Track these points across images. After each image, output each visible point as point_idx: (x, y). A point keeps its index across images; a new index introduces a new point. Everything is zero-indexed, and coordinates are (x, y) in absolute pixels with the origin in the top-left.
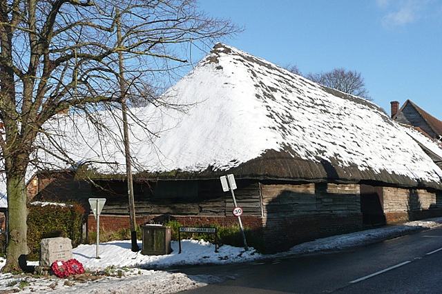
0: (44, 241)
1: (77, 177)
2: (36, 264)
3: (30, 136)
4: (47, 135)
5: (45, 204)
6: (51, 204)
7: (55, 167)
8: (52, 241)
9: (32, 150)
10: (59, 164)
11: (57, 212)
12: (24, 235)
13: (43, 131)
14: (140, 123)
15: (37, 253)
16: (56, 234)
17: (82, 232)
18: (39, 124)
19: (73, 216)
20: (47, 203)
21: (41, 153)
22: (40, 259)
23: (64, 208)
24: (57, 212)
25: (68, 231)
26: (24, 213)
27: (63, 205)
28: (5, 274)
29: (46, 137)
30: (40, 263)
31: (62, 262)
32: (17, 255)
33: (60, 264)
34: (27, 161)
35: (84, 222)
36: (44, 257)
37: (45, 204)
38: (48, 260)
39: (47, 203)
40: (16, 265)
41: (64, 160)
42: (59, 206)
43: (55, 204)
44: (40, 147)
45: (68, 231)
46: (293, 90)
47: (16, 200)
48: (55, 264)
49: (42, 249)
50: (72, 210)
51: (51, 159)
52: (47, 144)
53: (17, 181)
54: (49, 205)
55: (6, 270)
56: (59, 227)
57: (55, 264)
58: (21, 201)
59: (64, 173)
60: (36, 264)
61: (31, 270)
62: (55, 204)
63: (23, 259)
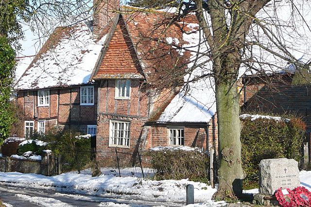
0: (264, 162)
1: (295, 81)
2: (255, 191)
3: (242, 29)
4: (263, 27)
5: (255, 117)
6: (263, 117)
7: (275, 69)
8: (273, 162)
9: (245, 45)
10: (274, 64)
11: (270, 128)
12: (237, 156)
13: (257, 22)
14: (117, 54)
15: (255, 179)
16: (272, 155)
17: (303, 155)
18: (253, 12)
19: (291, 133)
20: (258, 116)
21: (256, 50)
22: (260, 186)
23: (280, 123)
24: (270, 128)
25: (285, 153)
26: (237, 128)
27: (277, 118)
28: (218, 202)
29: (261, 31)
30: (260, 191)
31: (288, 189)
32: (231, 180)
33: (285, 192)
34: (239, 61)
35: (305, 141)
36: (265, 182)
37: (255, 117)
38: (270, 187)
39: (258, 116)
40: (230, 192)
41: (286, 59)
42: (274, 120)
43: (268, 117)
44: (254, 43)
45: (285, 153)
46: (36, 30)
47: (226, 111)
48: (279, 191)
49: (262, 172)
50: (289, 124)
51: (270, 58)
52: (265, 41)
53: (228, 87)
54: (260, 119)
55: (219, 196)
56: (274, 146)
57: (279, 191)
58: (233, 112)
59: (287, 76)
60: (255, 191)
61: (249, 198)
62: (268, 117)
63: (238, 185)
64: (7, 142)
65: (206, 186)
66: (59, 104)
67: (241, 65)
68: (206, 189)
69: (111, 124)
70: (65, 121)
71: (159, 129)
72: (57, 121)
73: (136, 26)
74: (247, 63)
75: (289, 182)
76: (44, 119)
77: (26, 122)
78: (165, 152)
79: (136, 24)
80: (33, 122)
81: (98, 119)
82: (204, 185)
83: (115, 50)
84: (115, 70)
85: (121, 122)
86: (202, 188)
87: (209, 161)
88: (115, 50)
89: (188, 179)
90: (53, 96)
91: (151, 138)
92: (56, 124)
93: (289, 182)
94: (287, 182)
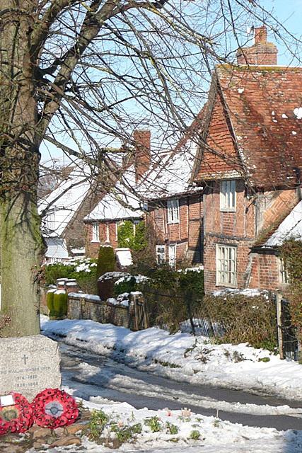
64: (103, 279)
65: (268, 356)
66: (190, 220)
67: (130, 169)
68: (267, 360)
69: (217, 249)
70: (195, 245)
71: (267, 257)
72: (187, 246)
73: (241, 94)
74: (93, 167)
75: (32, 381)
76: (175, 242)
77: (158, 247)
78: (225, 299)
79: (241, 91)
80: (164, 247)
81: (204, 243)
82: (265, 353)
83: (216, 134)
84: (217, 167)
85: (229, 247)
86: (260, 360)
87: (276, 314)
88: (216, 134)
89: (247, 343)
90: (182, 207)
91: (258, 272)
92: (187, 249)
93: (32, 381)
94: (27, 381)
